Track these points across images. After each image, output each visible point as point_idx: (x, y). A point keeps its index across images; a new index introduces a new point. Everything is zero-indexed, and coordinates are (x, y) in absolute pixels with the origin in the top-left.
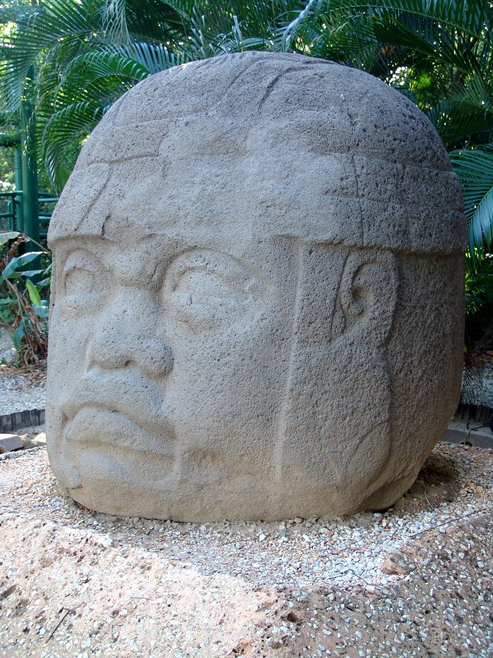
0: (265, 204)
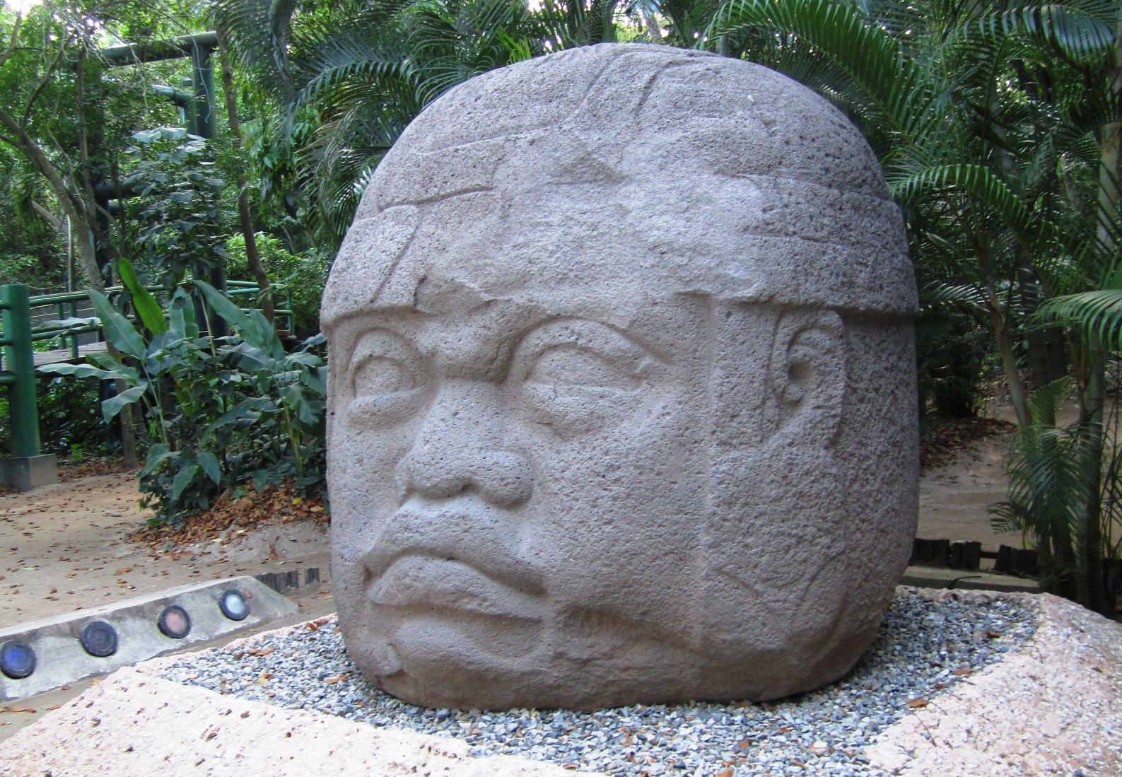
0: (658, 250)
